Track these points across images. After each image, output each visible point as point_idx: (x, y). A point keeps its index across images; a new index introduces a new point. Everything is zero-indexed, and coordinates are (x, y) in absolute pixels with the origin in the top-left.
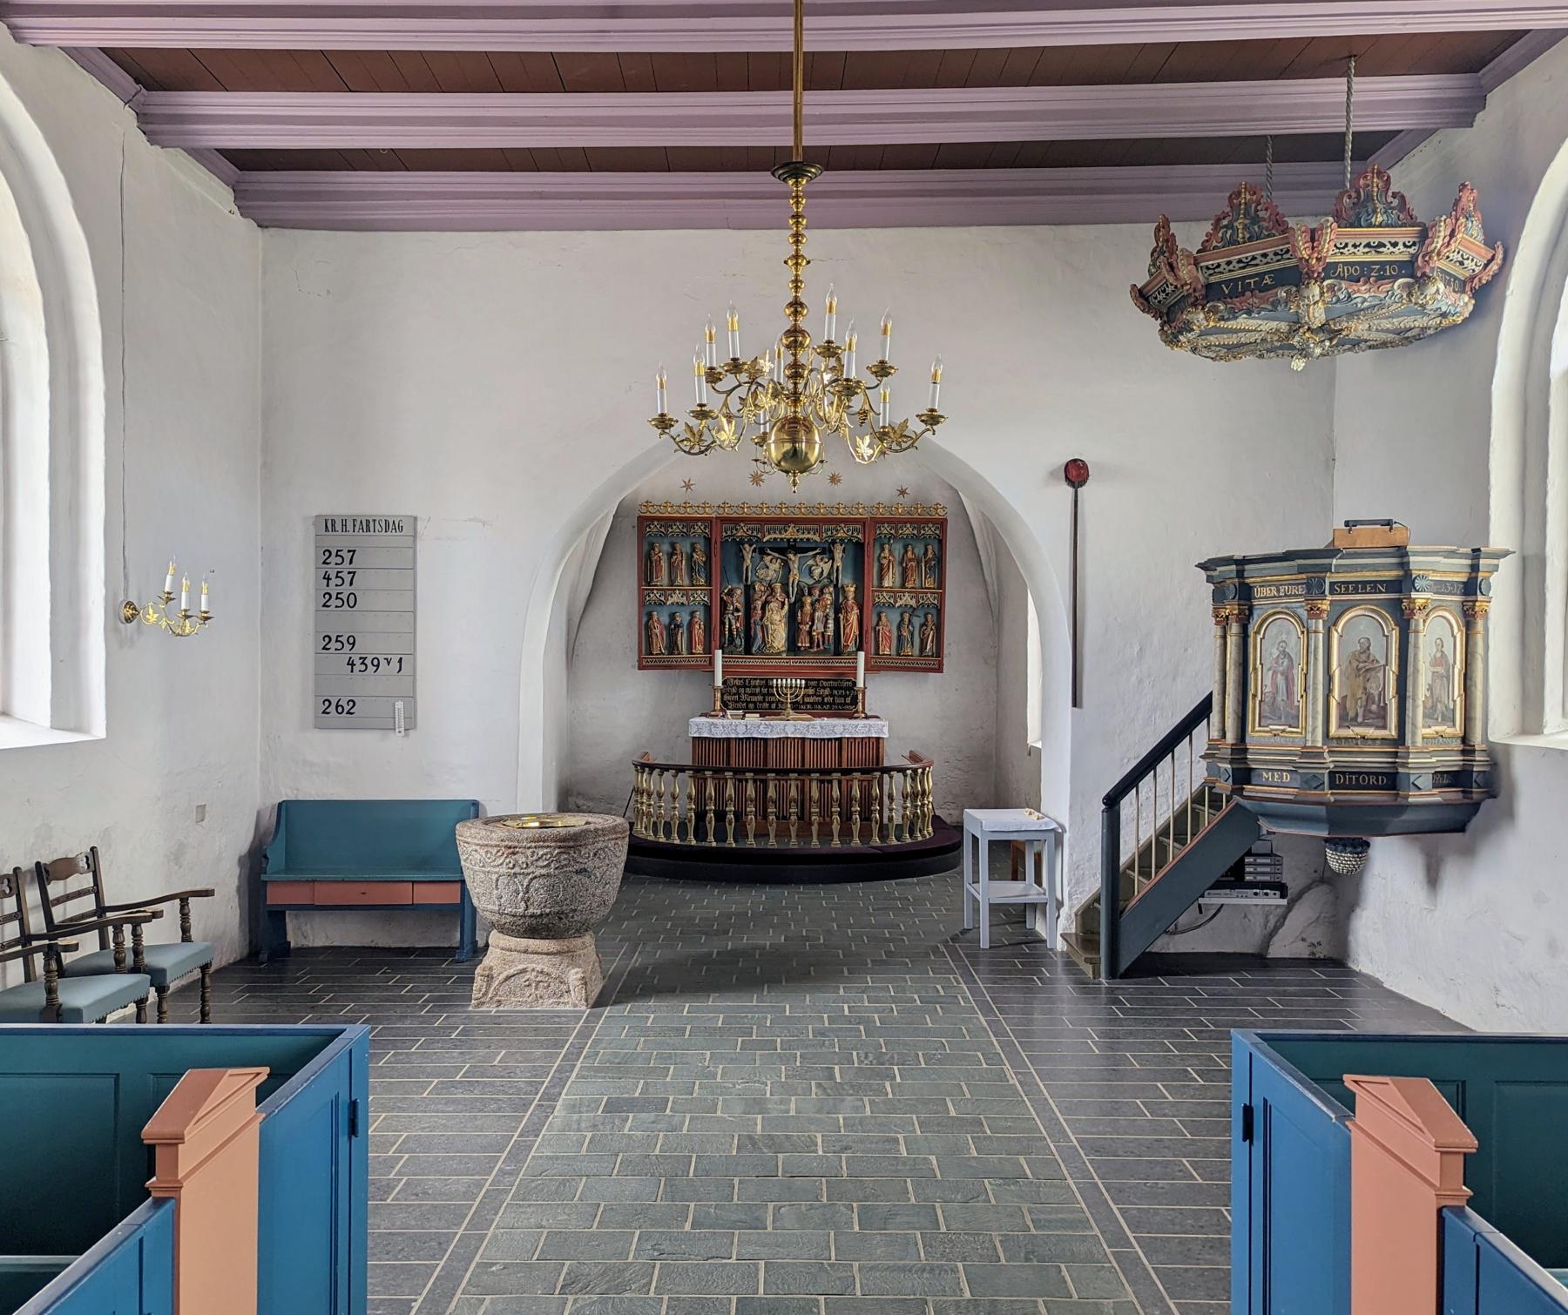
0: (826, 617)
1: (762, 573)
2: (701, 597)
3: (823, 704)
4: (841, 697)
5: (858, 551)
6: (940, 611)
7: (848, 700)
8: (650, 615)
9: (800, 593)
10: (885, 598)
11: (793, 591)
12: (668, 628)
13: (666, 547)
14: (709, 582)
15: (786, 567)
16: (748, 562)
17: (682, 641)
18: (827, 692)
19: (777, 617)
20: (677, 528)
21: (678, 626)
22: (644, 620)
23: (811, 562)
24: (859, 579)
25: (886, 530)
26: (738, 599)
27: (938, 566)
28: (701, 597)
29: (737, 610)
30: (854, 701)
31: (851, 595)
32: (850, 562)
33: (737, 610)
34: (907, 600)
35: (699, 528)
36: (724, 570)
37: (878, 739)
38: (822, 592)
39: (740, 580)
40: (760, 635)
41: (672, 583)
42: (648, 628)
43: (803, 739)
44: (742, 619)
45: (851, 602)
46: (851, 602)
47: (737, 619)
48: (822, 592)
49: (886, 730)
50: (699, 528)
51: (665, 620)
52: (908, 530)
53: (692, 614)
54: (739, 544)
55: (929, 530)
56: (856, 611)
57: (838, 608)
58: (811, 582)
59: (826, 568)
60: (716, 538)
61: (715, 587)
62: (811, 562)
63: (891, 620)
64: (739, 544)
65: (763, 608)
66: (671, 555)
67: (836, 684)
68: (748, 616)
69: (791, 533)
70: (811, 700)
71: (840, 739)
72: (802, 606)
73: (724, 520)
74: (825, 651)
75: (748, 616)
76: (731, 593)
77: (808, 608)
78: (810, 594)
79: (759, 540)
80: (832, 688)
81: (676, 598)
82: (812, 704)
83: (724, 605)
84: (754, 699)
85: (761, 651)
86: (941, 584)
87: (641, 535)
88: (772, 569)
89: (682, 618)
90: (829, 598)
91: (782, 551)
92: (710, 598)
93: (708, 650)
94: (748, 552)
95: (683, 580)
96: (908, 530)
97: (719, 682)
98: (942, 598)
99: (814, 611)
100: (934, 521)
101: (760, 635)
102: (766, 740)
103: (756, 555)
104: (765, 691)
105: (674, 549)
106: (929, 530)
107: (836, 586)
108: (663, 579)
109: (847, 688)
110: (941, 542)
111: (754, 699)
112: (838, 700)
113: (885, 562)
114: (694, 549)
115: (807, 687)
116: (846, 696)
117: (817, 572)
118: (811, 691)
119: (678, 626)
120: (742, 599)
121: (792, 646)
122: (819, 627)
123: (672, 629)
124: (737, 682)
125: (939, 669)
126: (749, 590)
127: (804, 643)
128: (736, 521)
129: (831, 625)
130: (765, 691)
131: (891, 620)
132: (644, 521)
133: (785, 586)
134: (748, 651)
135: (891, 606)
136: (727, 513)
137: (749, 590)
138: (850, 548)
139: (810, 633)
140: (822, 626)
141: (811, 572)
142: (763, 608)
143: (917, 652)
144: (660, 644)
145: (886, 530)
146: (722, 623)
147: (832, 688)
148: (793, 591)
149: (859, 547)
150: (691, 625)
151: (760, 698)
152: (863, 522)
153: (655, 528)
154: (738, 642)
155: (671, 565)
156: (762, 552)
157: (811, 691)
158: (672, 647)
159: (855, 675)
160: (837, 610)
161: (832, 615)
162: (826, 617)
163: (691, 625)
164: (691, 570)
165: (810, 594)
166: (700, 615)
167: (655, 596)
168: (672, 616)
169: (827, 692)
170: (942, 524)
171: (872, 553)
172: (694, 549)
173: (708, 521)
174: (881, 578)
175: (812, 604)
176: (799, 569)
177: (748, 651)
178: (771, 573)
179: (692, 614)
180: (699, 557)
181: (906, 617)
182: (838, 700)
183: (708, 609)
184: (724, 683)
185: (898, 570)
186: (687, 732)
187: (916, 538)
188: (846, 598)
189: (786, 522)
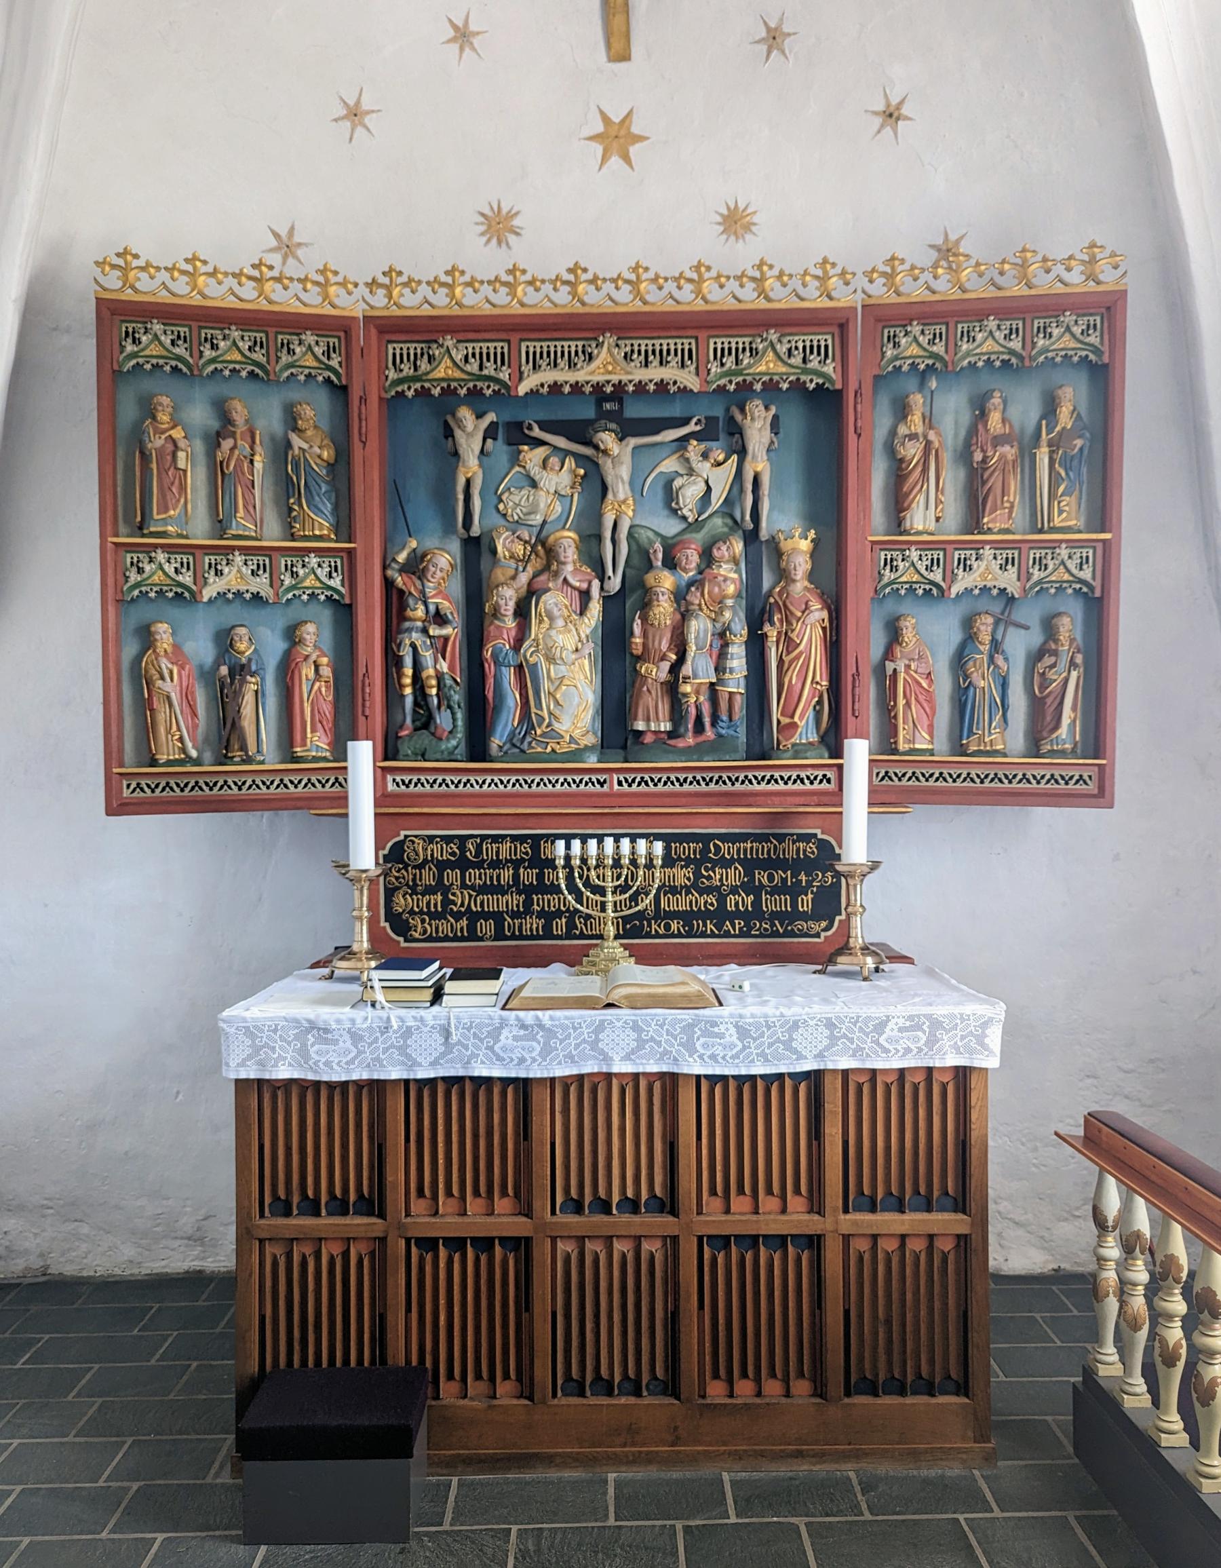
0: (723, 636)
1: (516, 501)
2: (319, 574)
3: (721, 915)
4: (780, 899)
5: (824, 407)
6: (1097, 606)
7: (806, 903)
8: (146, 637)
9: (641, 561)
10: (911, 568)
11: (616, 555)
12: (208, 675)
13: (200, 415)
14: (345, 526)
15: (595, 485)
16: (471, 464)
17: (259, 722)
18: (734, 876)
19: (565, 640)
20: (233, 348)
21: (240, 671)
22: (130, 650)
23: (670, 465)
24: (828, 507)
25: (911, 346)
26: (443, 584)
27: (1097, 462)
28: (319, 574)
29: (440, 618)
30: (830, 903)
31: (801, 565)
32: (793, 460)
33: (440, 618)
34: (987, 571)
35: (308, 353)
36: (395, 499)
37: (962, 1075)
38: (707, 558)
39: (448, 527)
40: (512, 698)
41: (220, 526)
42: (142, 680)
43: (671, 1081)
44: (456, 646)
45: (800, 586)
46: (800, 586)
47: (441, 647)
48: (707, 558)
49: (995, 1038)
50: (308, 353)
51: (202, 649)
52: (988, 342)
53: (292, 635)
54: (441, 406)
55: (1061, 340)
56: (818, 614)
57: (758, 614)
58: (671, 528)
59: (721, 480)
60: (369, 386)
61: (369, 544)
62: (670, 465)
63: (931, 636)
64: (441, 406)
65: (522, 611)
66: (214, 441)
67: (763, 850)
68: (475, 637)
69: (605, 366)
70: (681, 903)
71: (815, 1078)
72: (645, 605)
73: (391, 328)
74: (719, 746)
75: (475, 637)
76: (417, 566)
77: (664, 610)
78: (671, 563)
79: (504, 395)
80: (750, 865)
81: (236, 576)
82: (687, 917)
83: (395, 604)
84: (494, 903)
85: (517, 749)
86: (1102, 514)
87: (113, 376)
88: (546, 488)
89: (261, 642)
90: (729, 576)
91: (580, 432)
92: (351, 580)
93: (833, 741)
94: (470, 430)
95: (257, 518)
96: (988, 342)
97: (364, 853)
98: (1107, 557)
99: (685, 615)
100: (1080, 305)
101: (512, 698)
102: (524, 1086)
103: (498, 447)
104: (528, 876)
105: (226, 419)
106: (1061, 340)
107: (751, 537)
108: (188, 516)
109: (808, 865)
110: (1102, 374)
111: (494, 903)
112: (769, 904)
113: (912, 451)
114: (292, 420)
115: (668, 861)
116: (795, 891)
117: (690, 494)
118: (681, 876)
119: (240, 671)
120: (456, 587)
121: (617, 730)
122: (699, 667)
123: (226, 682)
124: (440, 852)
125: (1101, 795)
126: (476, 550)
127: (652, 719)
128: (426, 331)
129: (738, 661)
130: (528, 876)
131: (931, 636)
132: (119, 317)
133: (590, 541)
134: (477, 749)
135: (934, 594)
136: (411, 303)
137: (476, 550)
138: (795, 420)
139: (672, 689)
140: (712, 664)
141: (670, 496)
142: (522, 611)
143: (941, 743)
144: (182, 731)
145: (911, 346)
146: (392, 661)
147: (750, 865)
148: (616, 555)
149: (824, 407)
150: (287, 669)
151: (515, 900)
152: (838, 323)
153: (156, 342)
154: (443, 720)
155: (218, 472)
156: (516, 435)
157: (681, 876)
158: (227, 736)
159: (836, 821)
160: (757, 618)
161: (740, 630)
162: (723, 636)
163: (287, 669)
164: (288, 488)
165: (671, 563)
166: (316, 635)
167: (161, 569)
168: (224, 640)
169: (734, 876)
170: (1108, 310)
171: (872, 422)
172: (292, 420)
173: (336, 328)
174: (898, 505)
175: (680, 596)
176: (637, 485)
177: (477, 749)
178: (543, 499)
179: (292, 635)
180: (314, 448)
181: (985, 627)
182: (769, 904)
183: (344, 611)
184: (394, 856)
185: (952, 479)
186: (217, 1064)
187: (1010, 367)
188: (783, 575)
189: (586, 328)
